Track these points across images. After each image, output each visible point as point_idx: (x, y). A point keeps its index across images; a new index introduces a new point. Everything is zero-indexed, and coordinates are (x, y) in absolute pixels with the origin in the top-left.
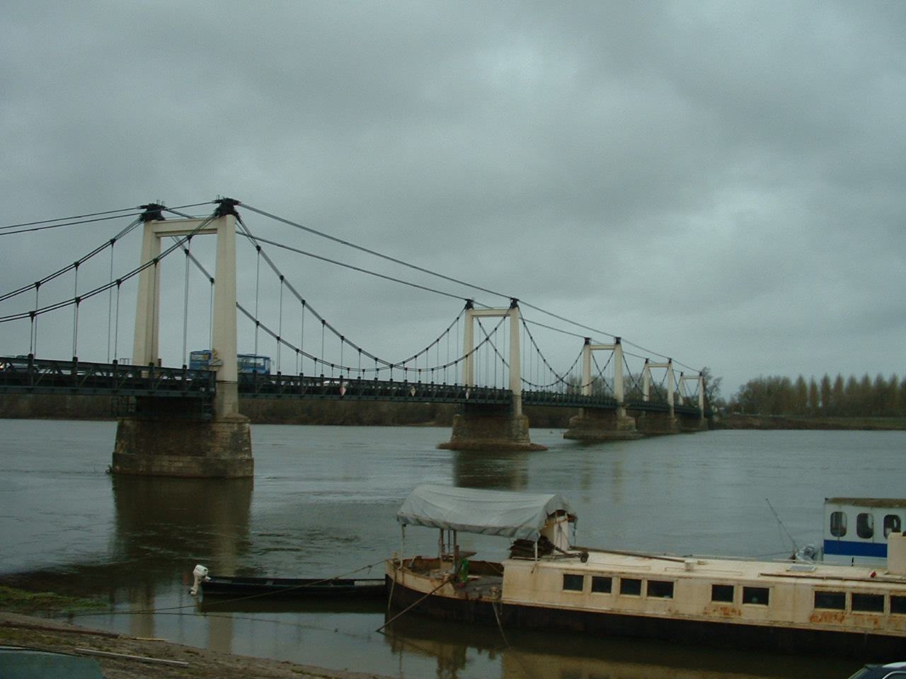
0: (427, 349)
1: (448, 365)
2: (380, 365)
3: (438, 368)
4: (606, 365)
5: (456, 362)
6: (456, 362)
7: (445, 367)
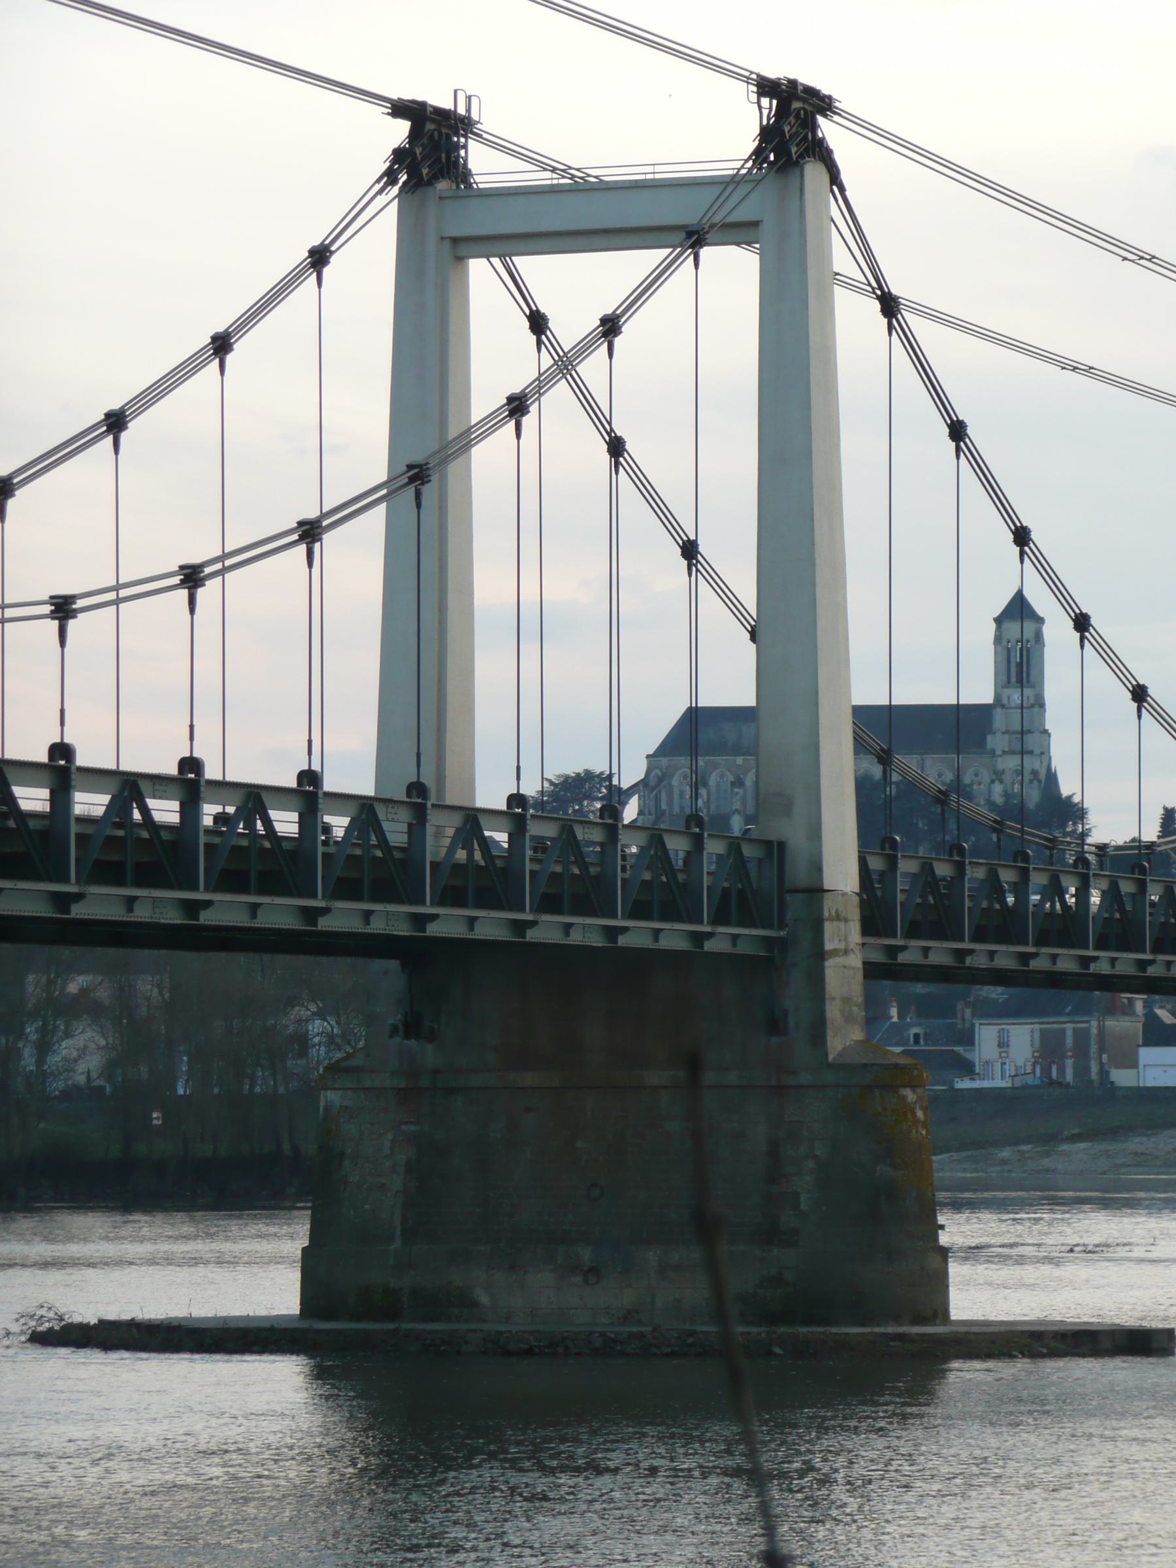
0: (221, 345)
7: (192, 577)
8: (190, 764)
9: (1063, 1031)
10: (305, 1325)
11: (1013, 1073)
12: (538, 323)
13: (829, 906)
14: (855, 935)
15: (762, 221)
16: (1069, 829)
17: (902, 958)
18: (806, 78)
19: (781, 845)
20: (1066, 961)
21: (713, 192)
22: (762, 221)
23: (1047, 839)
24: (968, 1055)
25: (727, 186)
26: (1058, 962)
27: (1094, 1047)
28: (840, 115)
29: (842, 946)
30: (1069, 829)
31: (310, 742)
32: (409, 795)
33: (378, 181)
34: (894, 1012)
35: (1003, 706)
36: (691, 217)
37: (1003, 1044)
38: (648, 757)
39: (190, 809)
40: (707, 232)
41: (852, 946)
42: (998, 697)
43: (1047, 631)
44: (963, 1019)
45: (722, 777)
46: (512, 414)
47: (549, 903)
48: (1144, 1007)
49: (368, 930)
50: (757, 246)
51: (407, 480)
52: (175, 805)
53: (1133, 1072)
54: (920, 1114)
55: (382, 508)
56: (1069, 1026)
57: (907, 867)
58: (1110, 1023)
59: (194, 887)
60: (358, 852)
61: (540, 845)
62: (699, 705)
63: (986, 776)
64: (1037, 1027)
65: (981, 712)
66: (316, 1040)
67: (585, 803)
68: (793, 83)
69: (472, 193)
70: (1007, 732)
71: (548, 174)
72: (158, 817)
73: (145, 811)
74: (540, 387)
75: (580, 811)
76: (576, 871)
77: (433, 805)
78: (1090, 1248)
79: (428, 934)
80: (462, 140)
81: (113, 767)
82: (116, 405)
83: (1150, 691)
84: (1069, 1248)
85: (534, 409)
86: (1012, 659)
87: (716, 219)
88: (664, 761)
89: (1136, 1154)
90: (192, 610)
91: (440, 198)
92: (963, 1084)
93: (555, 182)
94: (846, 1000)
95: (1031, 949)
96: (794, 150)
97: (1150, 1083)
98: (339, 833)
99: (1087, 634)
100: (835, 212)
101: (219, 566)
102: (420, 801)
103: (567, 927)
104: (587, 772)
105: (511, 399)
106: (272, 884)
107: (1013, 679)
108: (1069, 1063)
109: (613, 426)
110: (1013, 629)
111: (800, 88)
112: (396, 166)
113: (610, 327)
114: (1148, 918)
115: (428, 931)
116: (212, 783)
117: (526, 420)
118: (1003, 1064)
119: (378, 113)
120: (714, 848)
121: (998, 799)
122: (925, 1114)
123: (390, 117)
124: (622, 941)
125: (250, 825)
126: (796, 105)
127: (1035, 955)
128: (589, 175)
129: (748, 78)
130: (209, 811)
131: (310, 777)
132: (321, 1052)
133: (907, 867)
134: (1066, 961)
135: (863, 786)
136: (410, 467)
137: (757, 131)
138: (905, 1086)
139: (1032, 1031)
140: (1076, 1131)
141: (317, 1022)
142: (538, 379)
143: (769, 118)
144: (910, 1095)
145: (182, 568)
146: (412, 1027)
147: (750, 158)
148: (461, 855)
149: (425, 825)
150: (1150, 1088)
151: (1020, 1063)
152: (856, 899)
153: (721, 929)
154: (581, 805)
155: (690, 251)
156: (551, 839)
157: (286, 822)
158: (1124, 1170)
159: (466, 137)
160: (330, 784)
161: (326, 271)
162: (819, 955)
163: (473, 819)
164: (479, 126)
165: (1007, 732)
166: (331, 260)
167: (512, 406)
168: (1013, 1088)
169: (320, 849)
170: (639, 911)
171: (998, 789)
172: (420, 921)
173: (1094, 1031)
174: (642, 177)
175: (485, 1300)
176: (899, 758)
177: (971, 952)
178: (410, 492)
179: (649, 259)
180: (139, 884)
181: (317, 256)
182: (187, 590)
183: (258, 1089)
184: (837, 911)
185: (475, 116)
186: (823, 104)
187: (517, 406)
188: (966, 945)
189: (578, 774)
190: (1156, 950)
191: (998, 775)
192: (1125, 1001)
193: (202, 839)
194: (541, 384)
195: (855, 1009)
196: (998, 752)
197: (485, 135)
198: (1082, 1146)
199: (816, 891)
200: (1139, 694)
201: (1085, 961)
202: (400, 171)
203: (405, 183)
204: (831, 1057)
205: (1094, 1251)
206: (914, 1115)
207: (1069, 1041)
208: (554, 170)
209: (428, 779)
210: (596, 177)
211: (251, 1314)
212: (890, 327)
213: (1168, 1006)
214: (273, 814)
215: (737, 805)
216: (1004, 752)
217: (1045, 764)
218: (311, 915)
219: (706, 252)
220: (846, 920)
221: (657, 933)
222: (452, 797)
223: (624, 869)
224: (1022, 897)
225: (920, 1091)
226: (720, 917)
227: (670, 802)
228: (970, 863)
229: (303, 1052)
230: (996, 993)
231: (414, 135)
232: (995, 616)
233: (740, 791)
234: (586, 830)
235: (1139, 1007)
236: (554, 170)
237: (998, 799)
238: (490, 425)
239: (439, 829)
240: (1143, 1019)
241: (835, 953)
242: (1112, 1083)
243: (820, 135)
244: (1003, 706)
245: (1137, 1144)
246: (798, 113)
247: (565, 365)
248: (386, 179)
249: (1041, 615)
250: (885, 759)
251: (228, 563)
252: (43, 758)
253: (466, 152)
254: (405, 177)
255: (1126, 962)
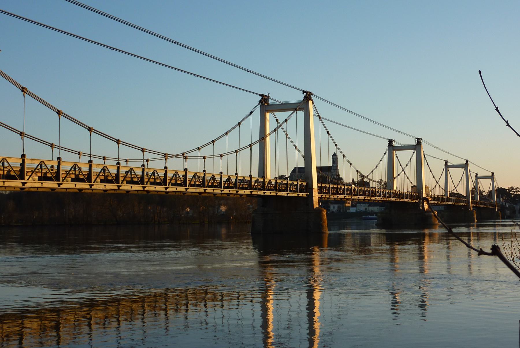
1: (240, 150)
2: (147, 155)
3: (227, 154)
6: (250, 146)
7: (236, 151)
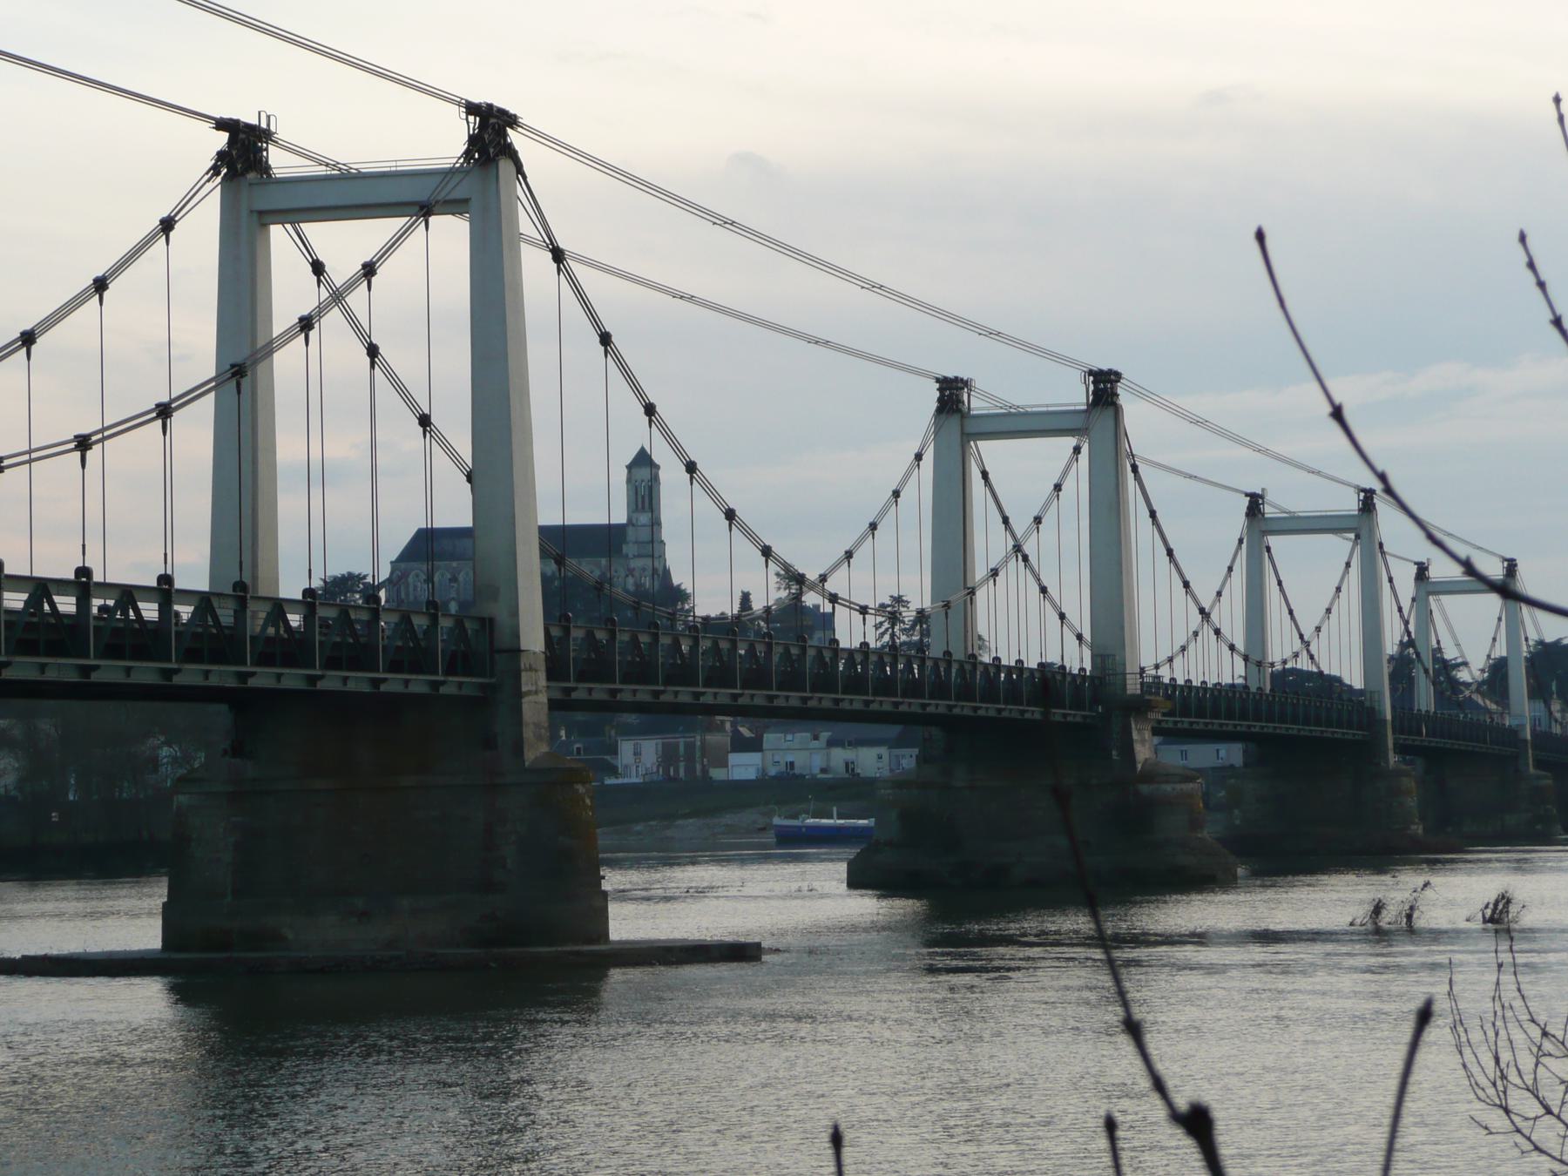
0: (100, 285)
1: (107, 433)
4: (1332, 603)
5: (164, 412)
6: (164, 412)
7: (83, 444)
8: (83, 572)
9: (677, 745)
10: (166, 955)
11: (644, 772)
12: (318, 268)
13: (524, 661)
14: (542, 681)
15: (470, 199)
16: (679, 607)
17: (663, 698)
18: (499, 103)
19: (491, 620)
20: (684, 695)
21: (438, 179)
22: (470, 199)
23: (669, 613)
24: (613, 762)
25: (445, 177)
26: (593, 694)
27: (698, 754)
28: (522, 127)
29: (534, 688)
30: (679, 607)
31: (166, 555)
32: (234, 590)
33: (207, 173)
34: (563, 733)
35: (633, 525)
36: (422, 195)
37: (637, 753)
38: (391, 562)
39: (83, 603)
40: (434, 206)
41: (540, 688)
42: (629, 519)
43: (662, 475)
44: (610, 737)
45: (443, 576)
46: (302, 330)
47: (332, 663)
48: (731, 726)
49: (406, 691)
50: (468, 215)
51: (230, 375)
52: (73, 600)
53: (725, 770)
54: (588, 801)
55: (212, 395)
56: (682, 740)
57: (577, 634)
58: (708, 737)
59: (87, 656)
60: (200, 630)
61: (324, 623)
62: (434, 526)
63: (622, 573)
64: (660, 741)
65: (620, 529)
66: (165, 760)
67: (349, 595)
68: (490, 106)
69: (272, 180)
70: (636, 542)
71: (324, 168)
72: (62, 608)
73: (52, 605)
74: (320, 308)
75: (345, 600)
76: (351, 641)
77: (251, 597)
78: (700, 890)
79: (249, 685)
80: (265, 145)
81: (28, 574)
82: (28, 327)
83: (737, 513)
84: (686, 890)
85: (317, 325)
86: (639, 493)
87: (439, 198)
88: (403, 565)
89: (727, 825)
90: (83, 466)
91: (250, 184)
92: (610, 781)
93: (329, 173)
94: (537, 725)
95: (871, 698)
96: (491, 150)
97: (736, 777)
98: (185, 617)
99: (695, 475)
100: (520, 193)
101: (100, 436)
102: (242, 594)
103: (345, 679)
104: (349, 574)
105: (301, 319)
106: (141, 653)
107: (640, 506)
108: (682, 765)
109: (372, 339)
110: (644, 473)
111: (495, 109)
112: (219, 163)
113: (369, 270)
114: (700, 663)
115: (249, 683)
116: (179, 591)
117: (312, 333)
118: (637, 767)
119: (206, 128)
120: (445, 623)
121: (631, 587)
122: (591, 802)
123: (214, 130)
124: (383, 688)
125: (125, 613)
126: (492, 121)
127: (663, 692)
128: (351, 168)
129: (460, 102)
130: (97, 602)
131: (165, 579)
132: (169, 769)
133: (577, 634)
134: (684, 695)
135: (546, 581)
136: (233, 366)
137: (467, 138)
138: (577, 783)
139: (657, 744)
140: (687, 811)
141: (165, 748)
142: (319, 307)
143: (474, 130)
144: (581, 789)
145: (76, 437)
146: (237, 750)
147: (462, 156)
148: (271, 631)
149: (246, 611)
150: (737, 780)
151: (649, 766)
152: (543, 656)
153: (450, 679)
154: (345, 596)
155: (422, 219)
156: (333, 619)
157: (150, 611)
158: (719, 836)
159: (267, 143)
160: (179, 584)
161: (172, 234)
162: (518, 695)
163: (279, 607)
164: (275, 135)
165: (636, 542)
166: (176, 227)
167: (302, 324)
168: (644, 783)
169: (174, 629)
170: (395, 667)
171: (630, 581)
172: (244, 677)
173: (698, 743)
174: (388, 169)
175: (290, 936)
176: (572, 562)
177: (620, 691)
178: (234, 382)
179: (396, 224)
180: (48, 654)
181: (166, 224)
182: (79, 453)
183: (125, 795)
184: (530, 665)
185: (273, 128)
186: (511, 120)
187: (306, 324)
188: (618, 686)
189: (343, 575)
190: (813, 690)
191: (631, 572)
192: (718, 722)
193: (92, 623)
194: (321, 310)
195: (543, 731)
196: (630, 556)
197: (280, 142)
198: (691, 821)
199: (516, 651)
200: (730, 515)
201: (697, 695)
202: (222, 166)
203: (225, 174)
204: (527, 764)
205: (700, 892)
206: (584, 802)
207: (682, 749)
208: (327, 165)
209: (247, 579)
210: (356, 169)
211: (128, 949)
212: (559, 270)
213: (747, 726)
214: (141, 605)
215: (453, 595)
216: (634, 556)
217: (662, 564)
218: (168, 674)
219: (432, 219)
220: (536, 671)
221: (407, 682)
222: (262, 592)
223: (383, 638)
224: (865, 668)
225: (587, 786)
226: (450, 670)
227: (407, 594)
228: (620, 630)
229: (156, 769)
230: (631, 719)
231: (231, 142)
232: (627, 464)
233: (455, 585)
234: (221, 601)
235: (728, 726)
236: (327, 165)
237: (631, 587)
238: (287, 337)
239: (254, 613)
240: (731, 734)
241: (529, 693)
242: (711, 778)
243: (509, 141)
244: (633, 525)
245: (728, 819)
246: (494, 126)
247: (337, 297)
248: (212, 171)
249: (658, 463)
250: (560, 561)
251: (106, 434)
252: (72, 576)
253: (267, 153)
254: (226, 170)
255: (723, 695)
